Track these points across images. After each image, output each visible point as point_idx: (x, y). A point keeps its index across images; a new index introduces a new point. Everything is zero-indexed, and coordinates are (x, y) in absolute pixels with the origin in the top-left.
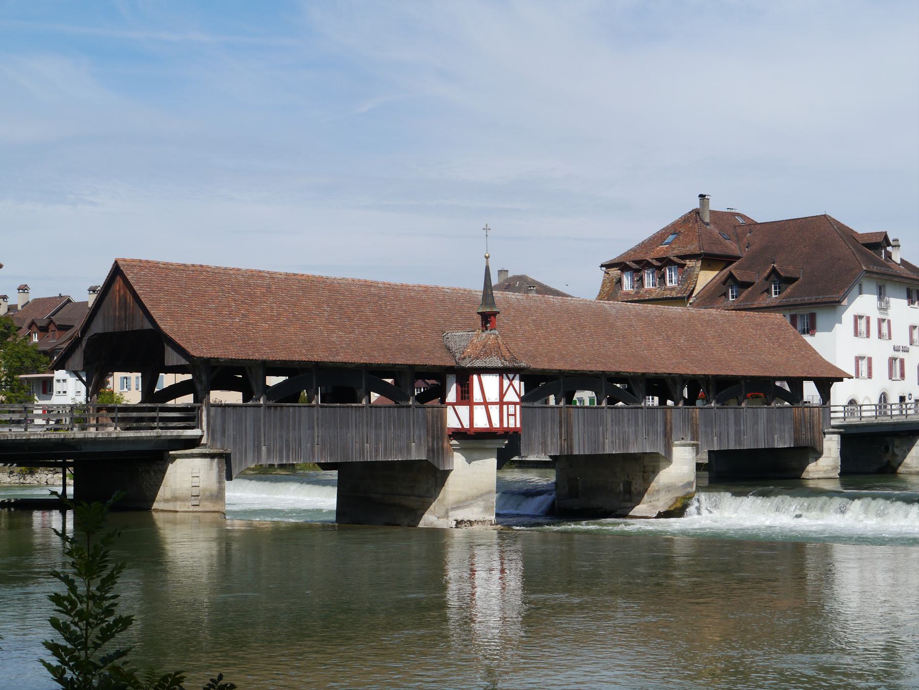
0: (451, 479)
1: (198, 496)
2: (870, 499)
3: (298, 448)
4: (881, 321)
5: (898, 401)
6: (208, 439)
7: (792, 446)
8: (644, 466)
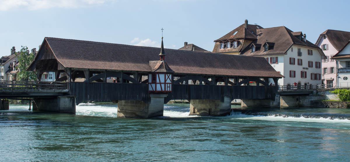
5: (304, 85)
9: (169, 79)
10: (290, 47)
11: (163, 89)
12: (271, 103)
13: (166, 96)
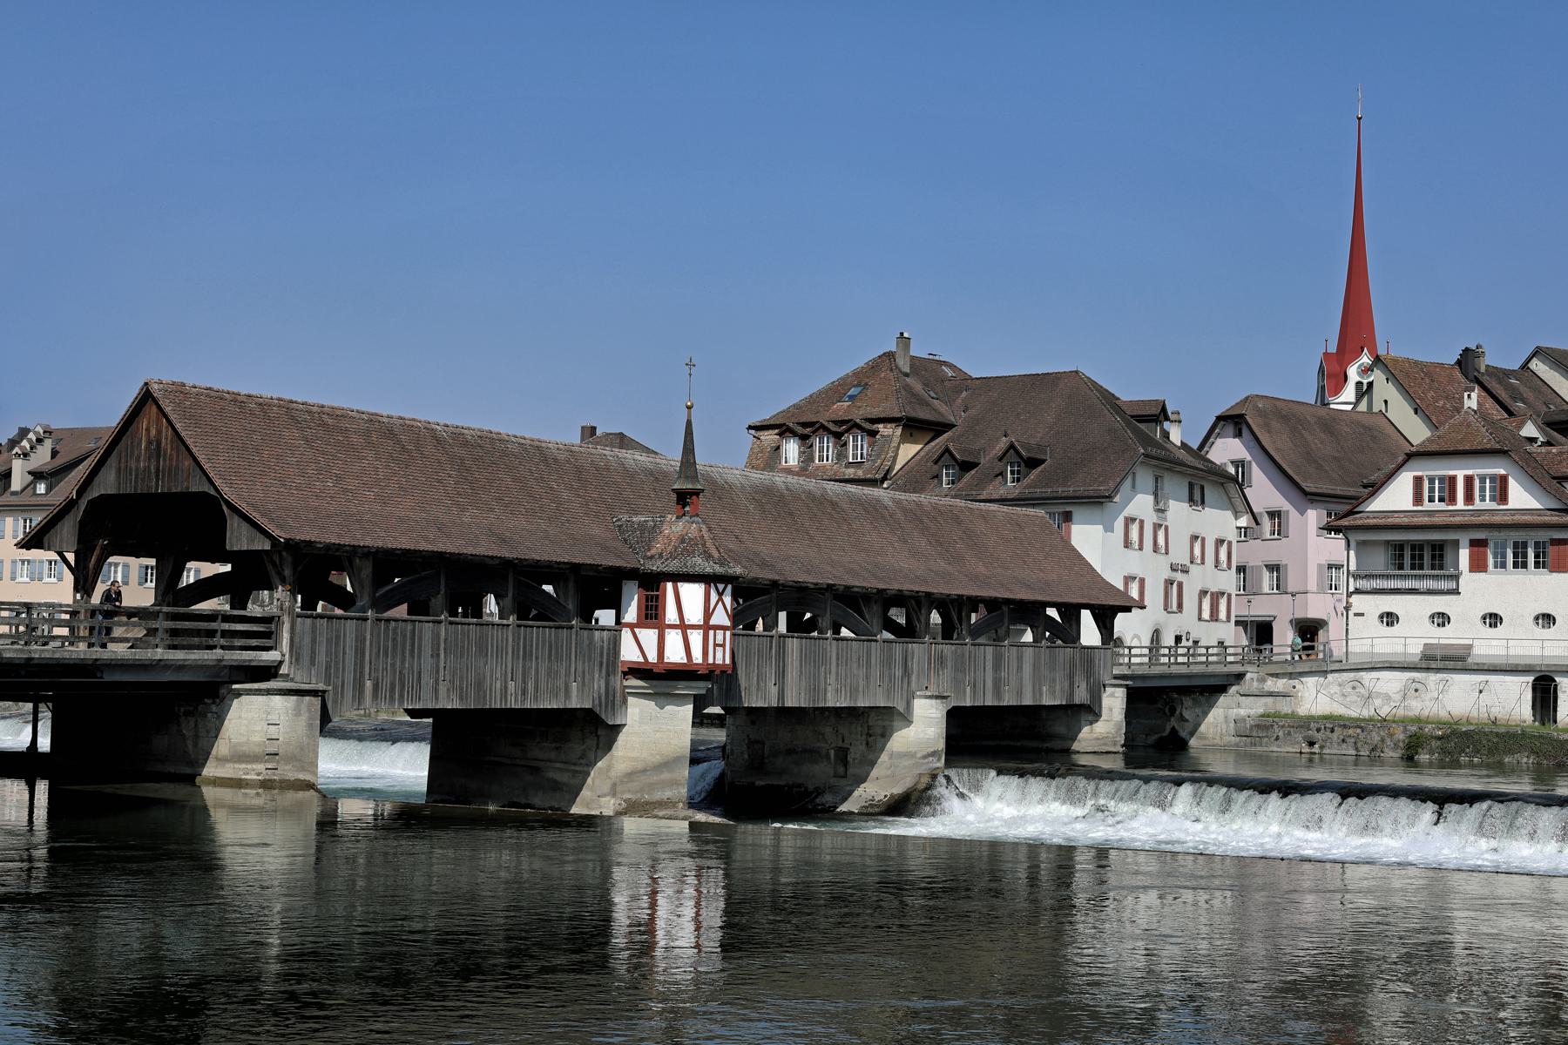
0: (622, 738)
1: (277, 754)
2: (1204, 785)
3: (417, 685)
4: (1157, 527)
6: (289, 667)
7: (1064, 703)
8: (868, 726)
11: (697, 656)
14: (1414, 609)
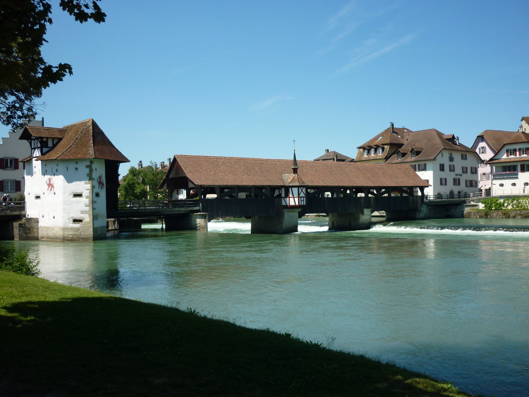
9: (303, 192)
10: (440, 152)
11: (297, 204)
12: (417, 214)
13: (299, 210)
14: (507, 183)
